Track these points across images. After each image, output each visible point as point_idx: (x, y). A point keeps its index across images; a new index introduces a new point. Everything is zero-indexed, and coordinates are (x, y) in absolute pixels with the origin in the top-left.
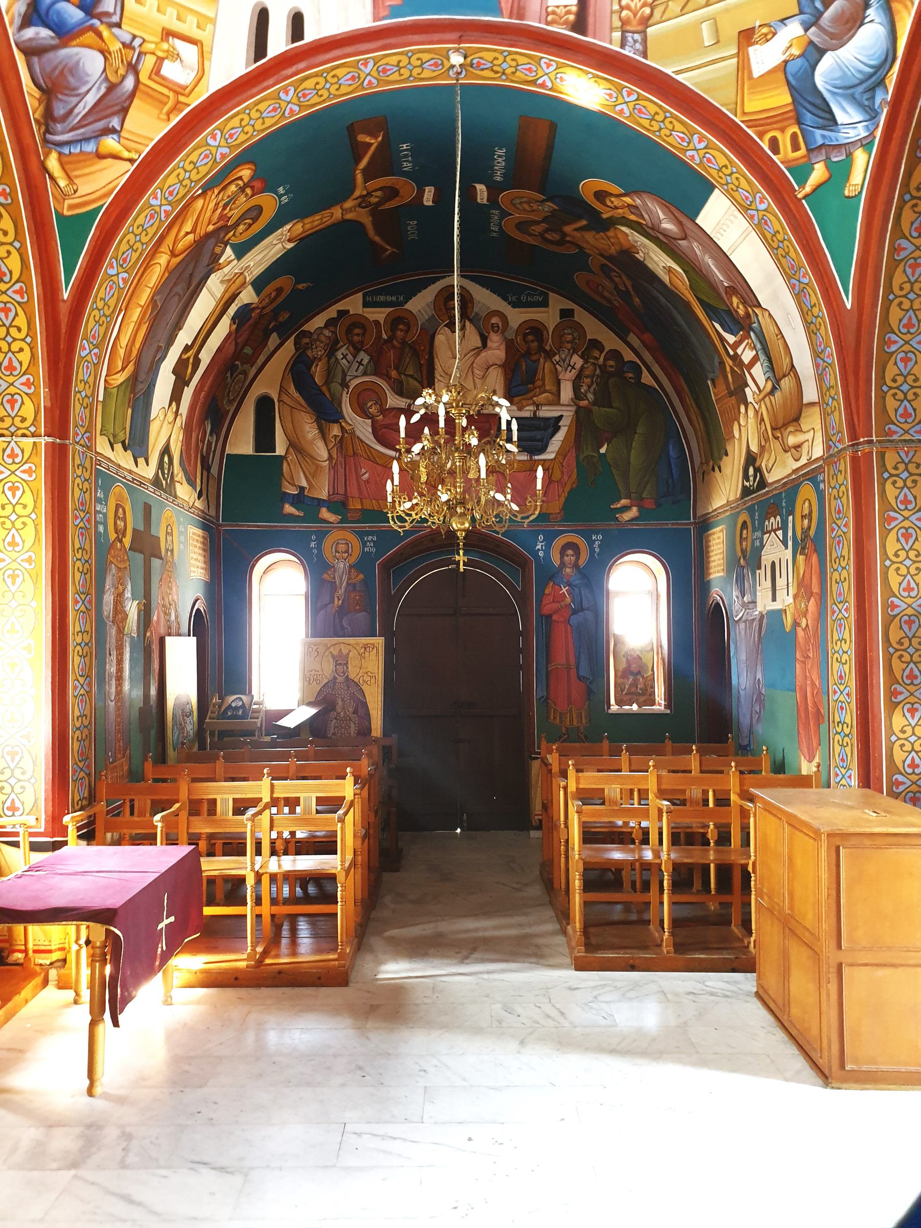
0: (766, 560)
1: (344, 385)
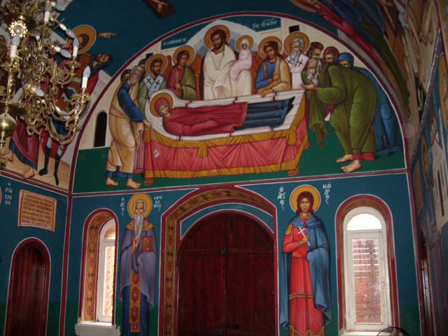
1: (148, 97)
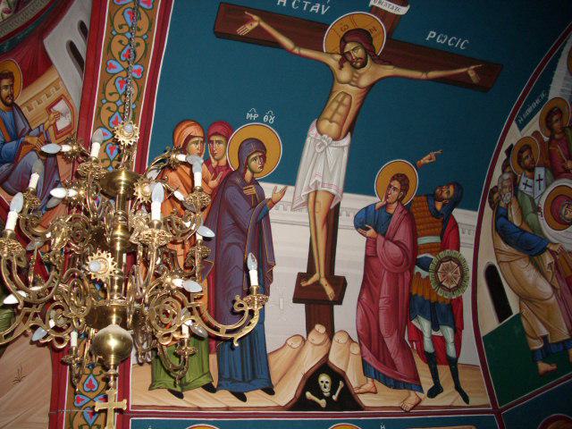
1: (537, 209)
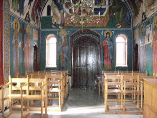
0: (147, 33)
